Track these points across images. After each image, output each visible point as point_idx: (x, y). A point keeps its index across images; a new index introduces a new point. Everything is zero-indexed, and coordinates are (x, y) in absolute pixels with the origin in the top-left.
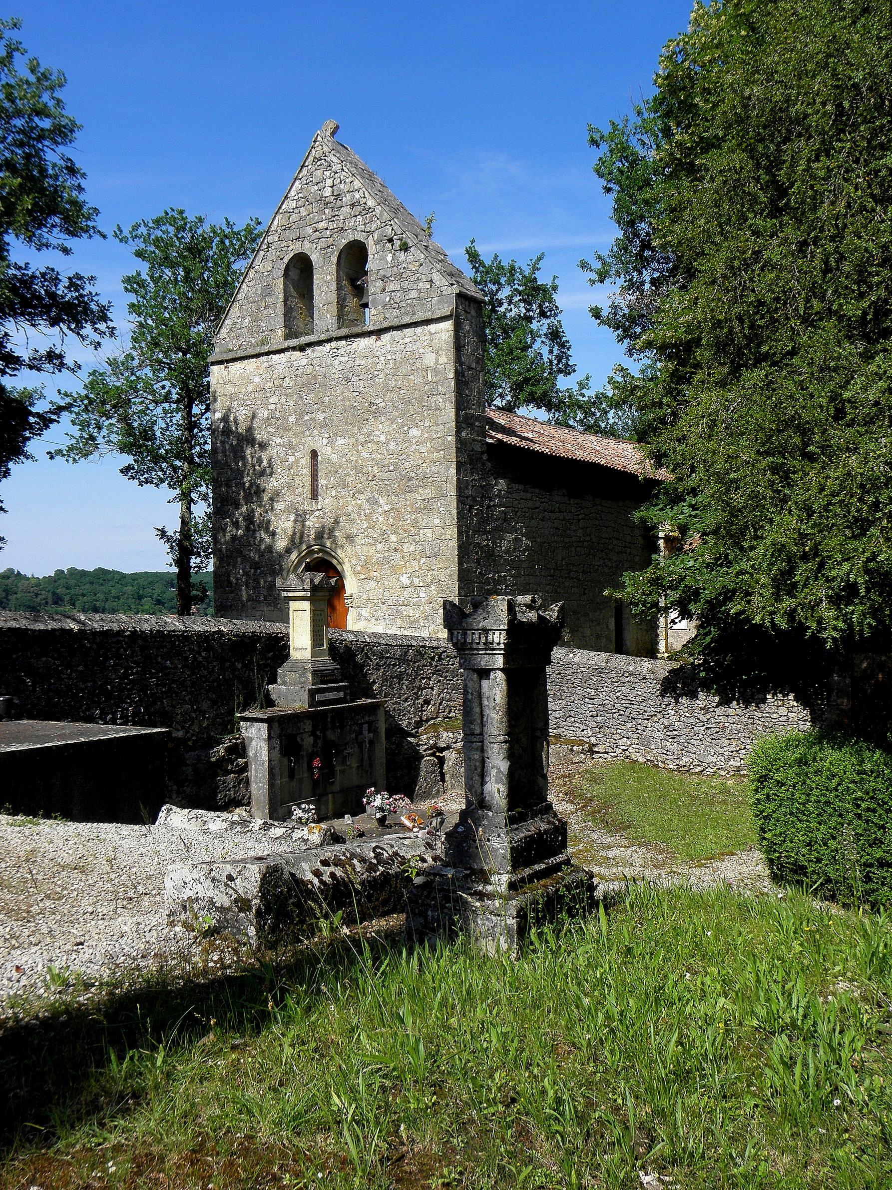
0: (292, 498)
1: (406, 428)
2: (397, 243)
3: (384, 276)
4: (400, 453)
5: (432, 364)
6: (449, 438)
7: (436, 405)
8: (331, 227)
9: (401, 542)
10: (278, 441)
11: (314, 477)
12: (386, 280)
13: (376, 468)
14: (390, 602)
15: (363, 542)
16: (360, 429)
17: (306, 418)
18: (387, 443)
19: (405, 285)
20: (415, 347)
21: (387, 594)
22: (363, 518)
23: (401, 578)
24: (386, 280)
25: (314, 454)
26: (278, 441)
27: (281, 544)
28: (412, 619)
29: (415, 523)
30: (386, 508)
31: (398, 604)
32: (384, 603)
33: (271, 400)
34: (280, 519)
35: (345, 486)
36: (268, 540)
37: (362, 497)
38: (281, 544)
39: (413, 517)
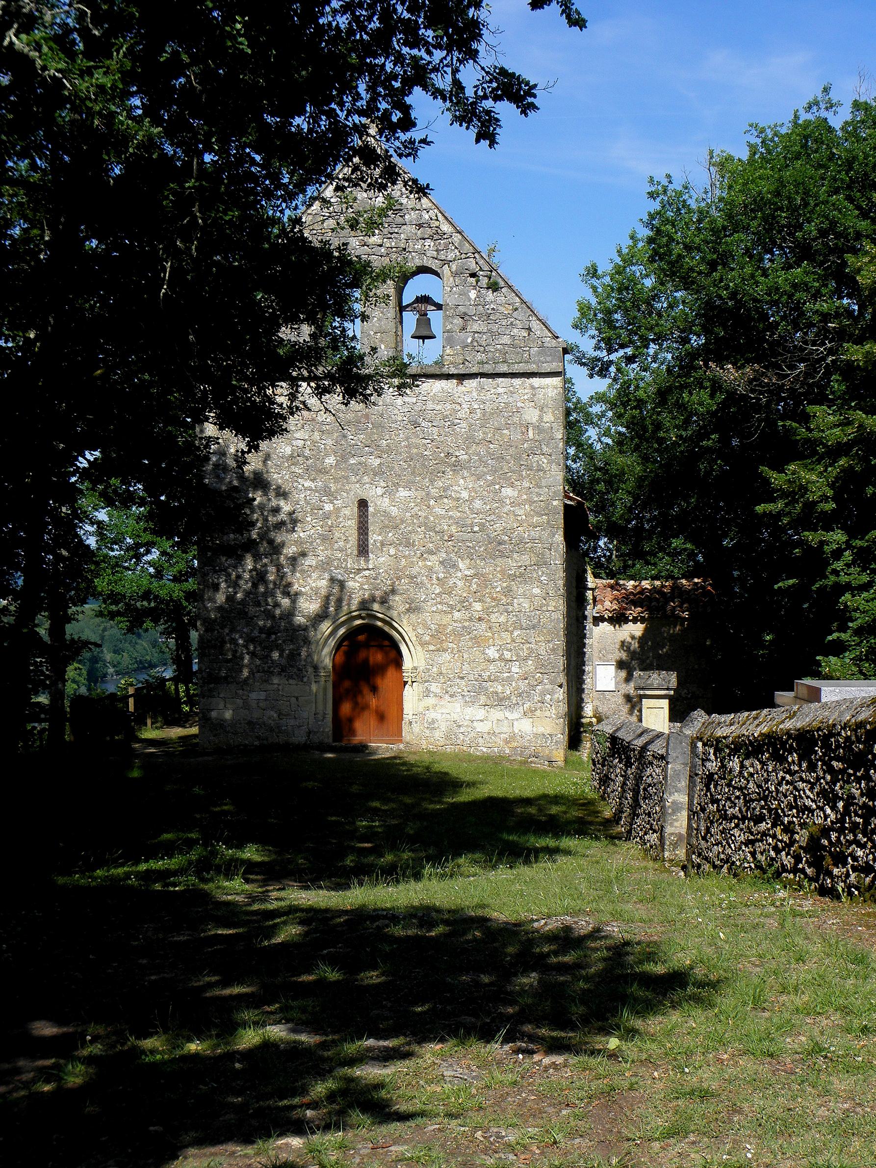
0: (329, 552)
1: (497, 487)
2: (484, 281)
3: (465, 314)
4: (491, 512)
5: (534, 420)
6: (555, 503)
7: (538, 465)
8: (388, 245)
9: (488, 611)
10: (308, 484)
11: (363, 529)
12: (467, 318)
13: (453, 527)
14: (471, 677)
15: (434, 609)
16: (432, 481)
17: (352, 461)
18: (471, 500)
19: (495, 327)
20: (511, 399)
21: (466, 667)
22: (435, 581)
23: (487, 651)
24: (467, 318)
25: (363, 504)
26: (308, 484)
27: (309, 606)
28: (501, 695)
29: (507, 592)
30: (468, 573)
31: (480, 679)
32: (462, 678)
33: (297, 435)
34: (310, 576)
35: (409, 544)
36: (285, 602)
37: (433, 558)
38: (309, 606)
39: (505, 585)
